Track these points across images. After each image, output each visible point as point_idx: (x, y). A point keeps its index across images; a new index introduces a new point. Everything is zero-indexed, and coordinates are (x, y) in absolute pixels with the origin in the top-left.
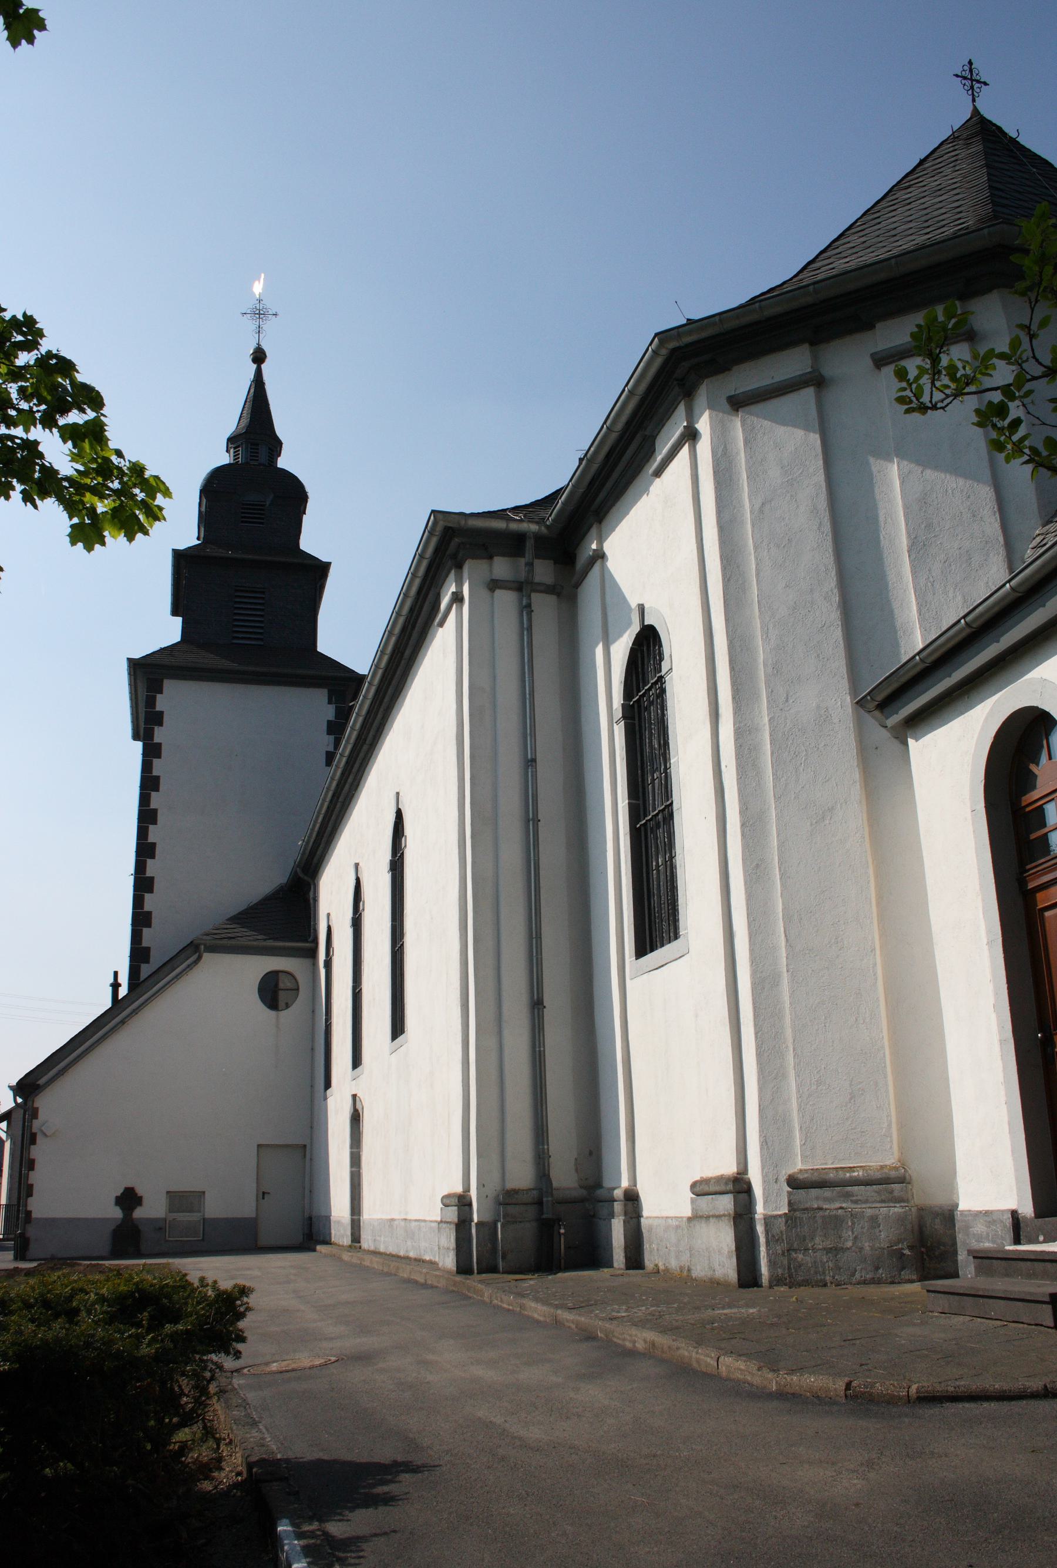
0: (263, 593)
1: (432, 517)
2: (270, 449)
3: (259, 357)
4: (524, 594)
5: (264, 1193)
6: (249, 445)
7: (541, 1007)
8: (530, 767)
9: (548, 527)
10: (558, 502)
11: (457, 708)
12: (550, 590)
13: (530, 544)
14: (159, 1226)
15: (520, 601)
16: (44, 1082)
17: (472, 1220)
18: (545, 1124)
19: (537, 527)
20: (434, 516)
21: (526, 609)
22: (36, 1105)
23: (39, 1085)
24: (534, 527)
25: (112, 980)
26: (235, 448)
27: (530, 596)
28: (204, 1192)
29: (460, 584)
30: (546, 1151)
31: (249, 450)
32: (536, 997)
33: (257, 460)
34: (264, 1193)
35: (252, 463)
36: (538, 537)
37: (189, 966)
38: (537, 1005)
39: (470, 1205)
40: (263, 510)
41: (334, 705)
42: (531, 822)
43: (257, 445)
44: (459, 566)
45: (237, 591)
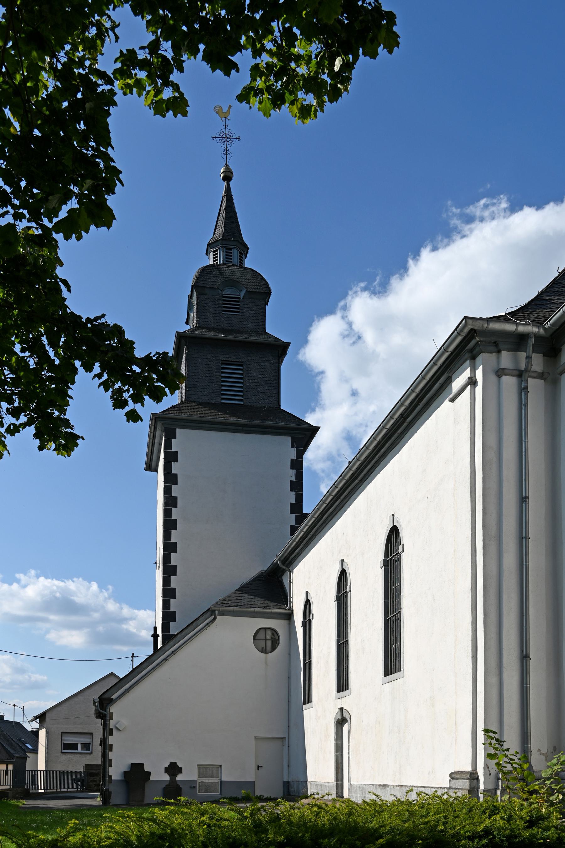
0: (242, 366)
1: (464, 322)
2: (240, 253)
3: (228, 177)
4: (523, 379)
5: (258, 766)
6: (225, 249)
7: (528, 659)
8: (524, 502)
9: (545, 329)
10: (560, 310)
11: (471, 461)
12: (541, 376)
13: (531, 342)
14: (192, 785)
15: (520, 384)
16: (116, 697)
17: (478, 788)
18: (529, 731)
19: (537, 330)
20: (466, 321)
21: (523, 390)
22: (111, 711)
23: (113, 699)
24: (535, 330)
25: (152, 633)
26: (214, 252)
27: (527, 381)
28: (221, 766)
29: (473, 370)
30: (529, 748)
31: (225, 254)
32: (524, 653)
33: (231, 262)
34: (258, 766)
35: (228, 263)
36: (537, 337)
37: (208, 624)
38: (524, 657)
39: (478, 779)
40: (238, 302)
41: (296, 448)
42: (524, 540)
43: (231, 249)
44: (473, 358)
45: (223, 364)
